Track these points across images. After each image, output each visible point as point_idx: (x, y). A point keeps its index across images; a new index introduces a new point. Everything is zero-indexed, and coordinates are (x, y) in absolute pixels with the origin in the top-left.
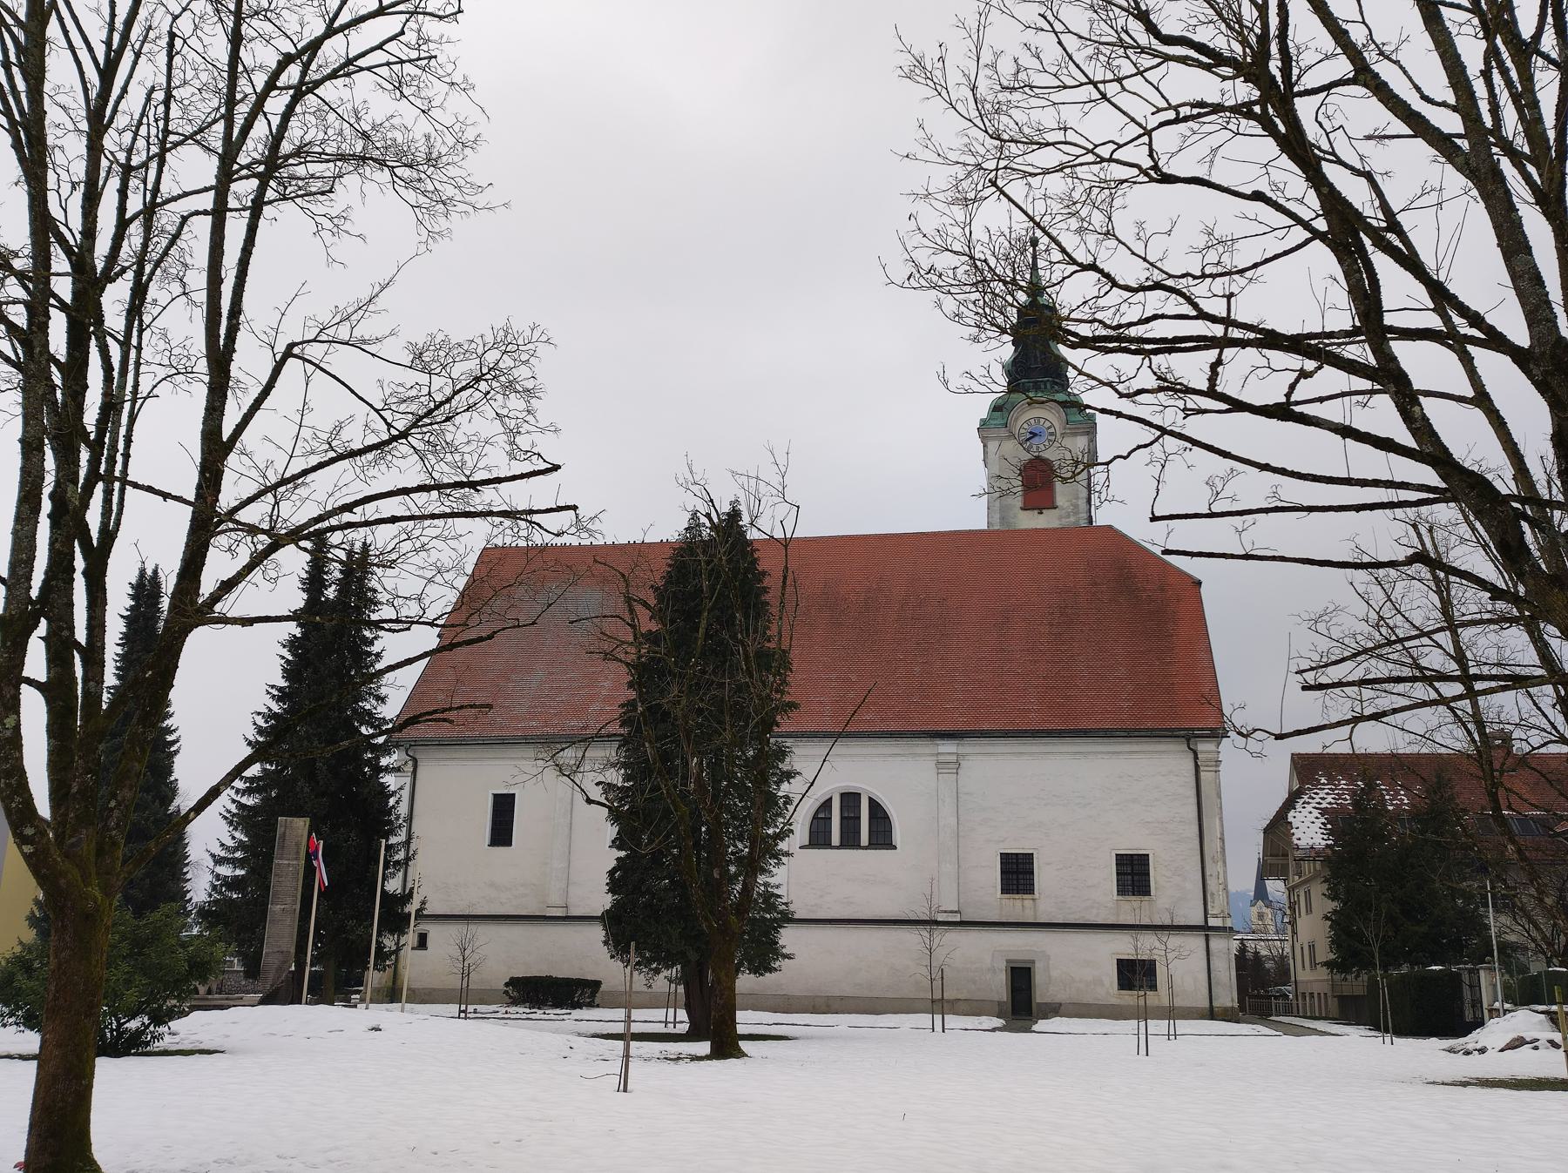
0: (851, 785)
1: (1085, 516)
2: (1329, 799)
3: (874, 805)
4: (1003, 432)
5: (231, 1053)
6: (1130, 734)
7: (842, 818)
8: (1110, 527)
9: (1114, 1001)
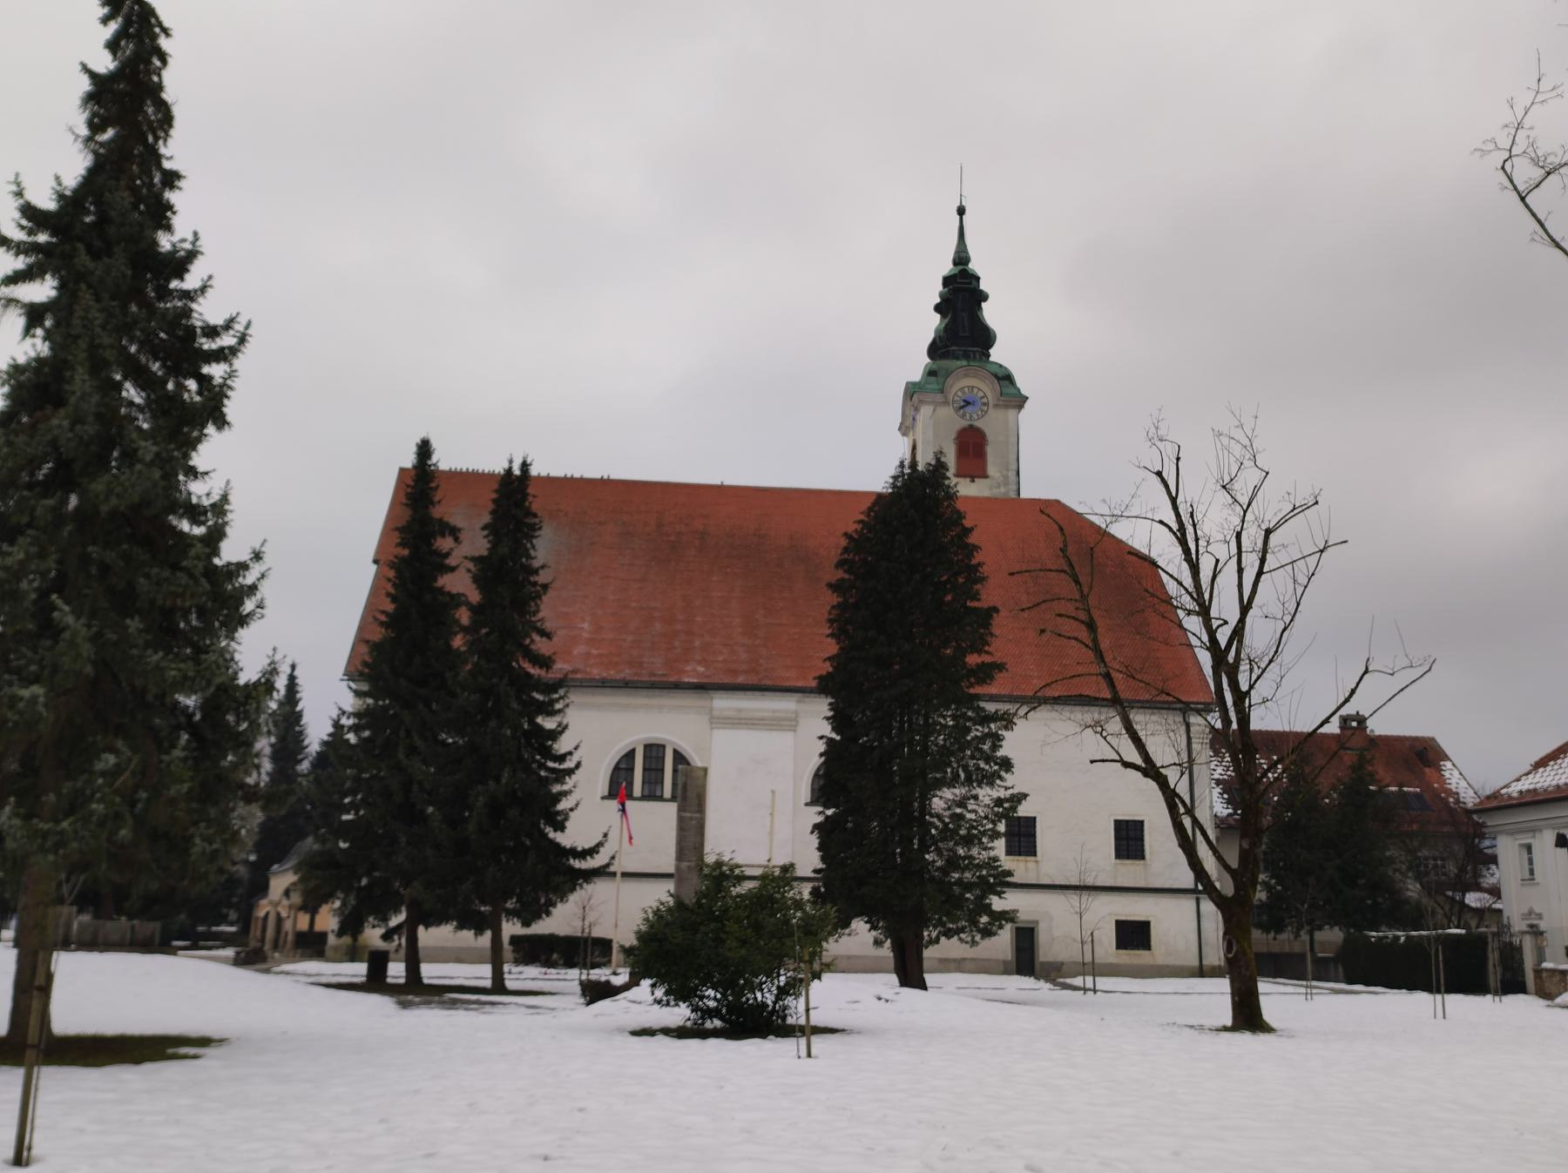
0: (655, 734)
1: (1014, 487)
2: (1220, 770)
3: (679, 758)
4: (939, 397)
5: (620, 1030)
6: (626, 685)
7: (662, 770)
8: (1058, 502)
9: (1113, 960)
